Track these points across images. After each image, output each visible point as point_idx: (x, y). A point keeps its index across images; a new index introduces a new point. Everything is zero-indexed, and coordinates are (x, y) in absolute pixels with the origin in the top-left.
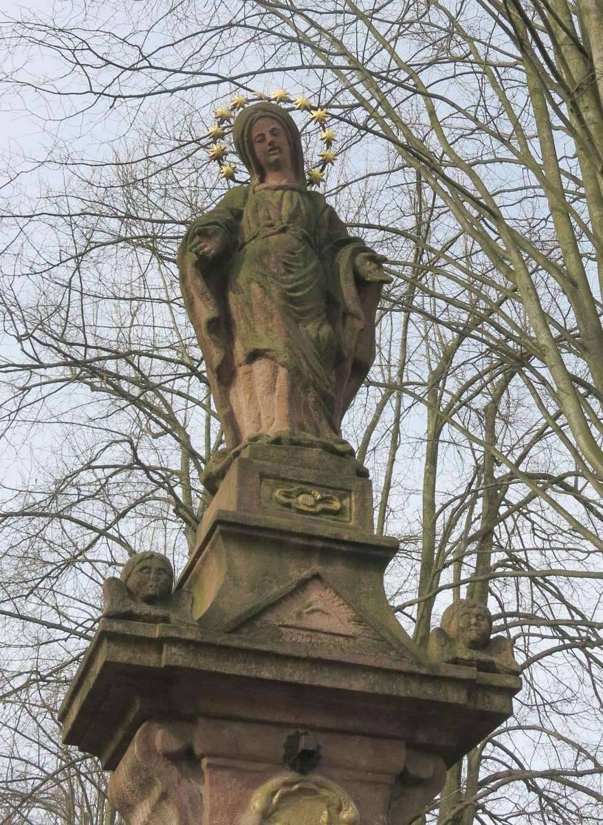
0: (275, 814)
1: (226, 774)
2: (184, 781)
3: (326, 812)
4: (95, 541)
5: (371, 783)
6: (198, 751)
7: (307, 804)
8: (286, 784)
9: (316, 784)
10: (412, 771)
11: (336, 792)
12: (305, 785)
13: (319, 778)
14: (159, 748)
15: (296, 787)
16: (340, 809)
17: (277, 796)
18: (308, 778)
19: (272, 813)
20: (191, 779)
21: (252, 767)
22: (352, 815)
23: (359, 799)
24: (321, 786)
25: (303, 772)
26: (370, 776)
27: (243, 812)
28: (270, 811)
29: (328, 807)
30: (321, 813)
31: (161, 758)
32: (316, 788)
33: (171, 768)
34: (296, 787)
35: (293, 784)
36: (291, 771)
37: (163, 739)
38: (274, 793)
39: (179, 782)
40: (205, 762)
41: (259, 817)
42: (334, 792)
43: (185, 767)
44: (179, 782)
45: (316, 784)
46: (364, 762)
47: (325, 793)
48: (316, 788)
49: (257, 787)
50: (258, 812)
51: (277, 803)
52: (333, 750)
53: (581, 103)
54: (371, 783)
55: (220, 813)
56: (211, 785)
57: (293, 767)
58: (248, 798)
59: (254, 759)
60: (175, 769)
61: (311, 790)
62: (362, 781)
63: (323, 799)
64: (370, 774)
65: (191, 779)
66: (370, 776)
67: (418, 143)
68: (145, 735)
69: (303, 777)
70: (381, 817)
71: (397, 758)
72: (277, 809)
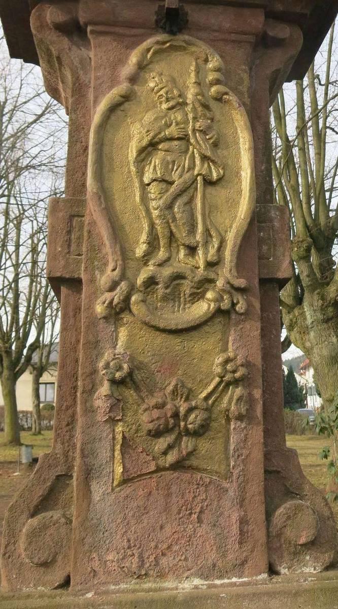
0: (150, 66)
1: (108, 38)
2: (74, 48)
3: (194, 63)
4: (34, 67)
5: (233, 41)
6: (82, 21)
7: (177, 57)
8: (158, 43)
9: (184, 41)
10: (271, 33)
11: (202, 48)
12: (175, 43)
13: (186, 37)
14: (49, 22)
15: (168, 44)
16: (206, 61)
17: (151, 53)
18: (177, 37)
19: (147, 65)
20: (81, 48)
21: (128, 32)
22: (216, 64)
23: (224, 54)
24: (189, 43)
25: (172, 33)
26: (233, 37)
27: (123, 66)
28: (145, 63)
29: (197, 59)
30: (191, 65)
31: (53, 30)
32: (184, 45)
33: (62, 38)
34: (168, 44)
35: (164, 43)
36: (164, 33)
37: (51, 14)
38: (148, 50)
39: (70, 49)
40: (89, 29)
41: (136, 67)
42: (201, 47)
43: (75, 39)
44: (70, 49)
45: (184, 41)
46: (227, 25)
47: (193, 49)
48: (184, 45)
49: (136, 48)
50: (135, 65)
51: (150, 58)
52: (196, 14)
53: (116, 301)
54: (233, 41)
55: (103, 67)
56: (95, 47)
57: (164, 30)
58: (127, 58)
59: (130, 25)
60: (66, 39)
61: (180, 46)
62: (225, 41)
63: (192, 53)
64: (233, 35)
65: (81, 48)
66: (233, 37)
67: (140, 117)
68: (37, 13)
69: (172, 37)
70: (244, 67)
71: (256, 21)
72: (151, 62)
